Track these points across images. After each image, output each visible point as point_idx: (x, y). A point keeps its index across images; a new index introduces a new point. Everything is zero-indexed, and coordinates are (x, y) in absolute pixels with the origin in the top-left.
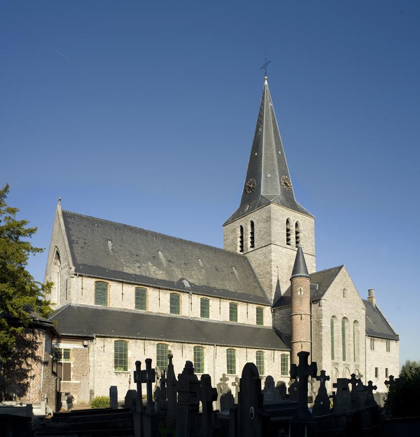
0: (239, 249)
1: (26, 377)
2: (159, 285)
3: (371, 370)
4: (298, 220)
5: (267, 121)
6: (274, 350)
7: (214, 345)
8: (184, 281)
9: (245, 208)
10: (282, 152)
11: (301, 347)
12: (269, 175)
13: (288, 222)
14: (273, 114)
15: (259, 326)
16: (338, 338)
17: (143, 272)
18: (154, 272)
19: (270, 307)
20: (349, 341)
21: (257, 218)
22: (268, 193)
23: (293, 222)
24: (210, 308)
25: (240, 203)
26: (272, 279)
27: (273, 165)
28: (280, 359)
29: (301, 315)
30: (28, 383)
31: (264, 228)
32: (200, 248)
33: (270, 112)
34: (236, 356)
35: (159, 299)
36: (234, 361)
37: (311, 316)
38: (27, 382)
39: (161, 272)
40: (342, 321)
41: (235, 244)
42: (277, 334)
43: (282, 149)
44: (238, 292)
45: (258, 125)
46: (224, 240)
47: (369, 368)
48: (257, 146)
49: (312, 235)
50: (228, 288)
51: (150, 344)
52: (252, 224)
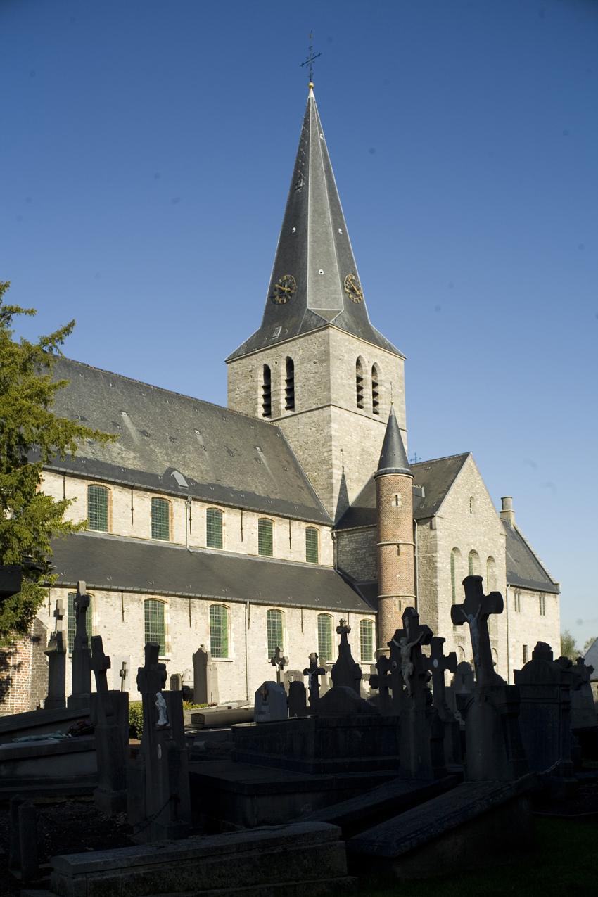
0: (261, 410)
1: (6, 667)
2: (132, 481)
3: (516, 649)
4: (376, 361)
5: (315, 169)
6: (348, 612)
7: (245, 603)
8: (175, 473)
9: (273, 331)
10: (344, 231)
13: (358, 363)
14: (325, 156)
15: (311, 565)
17: (100, 454)
18: (119, 454)
23: (367, 364)
24: (224, 528)
25: (262, 319)
27: (328, 253)
28: (359, 629)
29: (398, 545)
30: (9, 679)
32: (195, 408)
33: (321, 152)
34: (283, 623)
35: (132, 510)
36: (280, 633)
38: (8, 677)
39: (132, 455)
40: (469, 558)
41: (251, 400)
42: (346, 581)
43: (344, 226)
44: (273, 496)
45: (296, 174)
46: (230, 391)
47: (514, 646)
48: (295, 213)
49: (401, 391)
50: (253, 488)
51: (133, 600)
52: (290, 365)
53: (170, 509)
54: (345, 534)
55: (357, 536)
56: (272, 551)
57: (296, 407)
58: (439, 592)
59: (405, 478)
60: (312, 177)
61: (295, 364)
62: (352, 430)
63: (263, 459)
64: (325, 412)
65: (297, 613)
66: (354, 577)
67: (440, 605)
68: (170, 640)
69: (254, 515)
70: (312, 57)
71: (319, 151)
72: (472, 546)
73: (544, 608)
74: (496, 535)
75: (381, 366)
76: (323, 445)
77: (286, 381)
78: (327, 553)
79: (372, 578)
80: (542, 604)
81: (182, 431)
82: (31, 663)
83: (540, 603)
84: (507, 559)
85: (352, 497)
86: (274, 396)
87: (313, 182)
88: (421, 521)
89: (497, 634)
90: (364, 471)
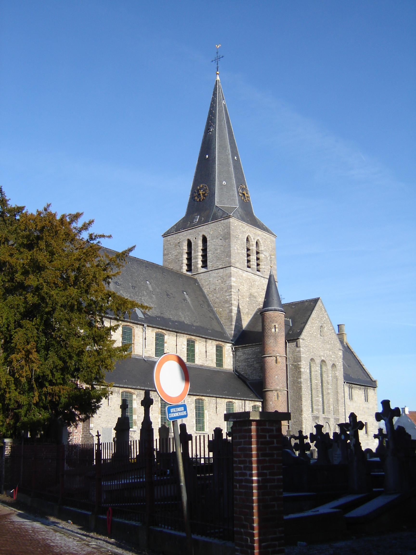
0: (185, 268)
4: (259, 238)
5: (220, 121)
11: (276, 396)
12: (224, 183)
13: (247, 239)
15: (218, 369)
16: (317, 385)
19: (231, 345)
20: (328, 389)
21: (211, 233)
22: (224, 204)
24: (165, 345)
26: (232, 309)
31: (222, 246)
32: (146, 267)
34: (205, 408)
37: (286, 358)
41: (179, 261)
44: (195, 324)
53: (133, 332)
54: (240, 349)
55: (249, 350)
56: (195, 360)
57: (208, 266)
58: (302, 388)
59: (280, 314)
60: (218, 126)
61: (208, 239)
62: (244, 282)
63: (188, 300)
64: (227, 271)
65: (214, 401)
66: (247, 377)
67: (303, 396)
68: (136, 418)
69: (184, 336)
70: (218, 58)
71: (223, 110)
72: (322, 357)
73: (367, 397)
74: (337, 350)
75: (261, 241)
76: (226, 291)
77: (202, 250)
78: (229, 361)
79: (258, 378)
80: (366, 394)
81: (139, 282)
82: (81, 434)
83: (365, 394)
84: (344, 365)
85: (245, 323)
86: (194, 259)
87: (219, 129)
88: (290, 342)
89: (339, 414)
90: (251, 308)
